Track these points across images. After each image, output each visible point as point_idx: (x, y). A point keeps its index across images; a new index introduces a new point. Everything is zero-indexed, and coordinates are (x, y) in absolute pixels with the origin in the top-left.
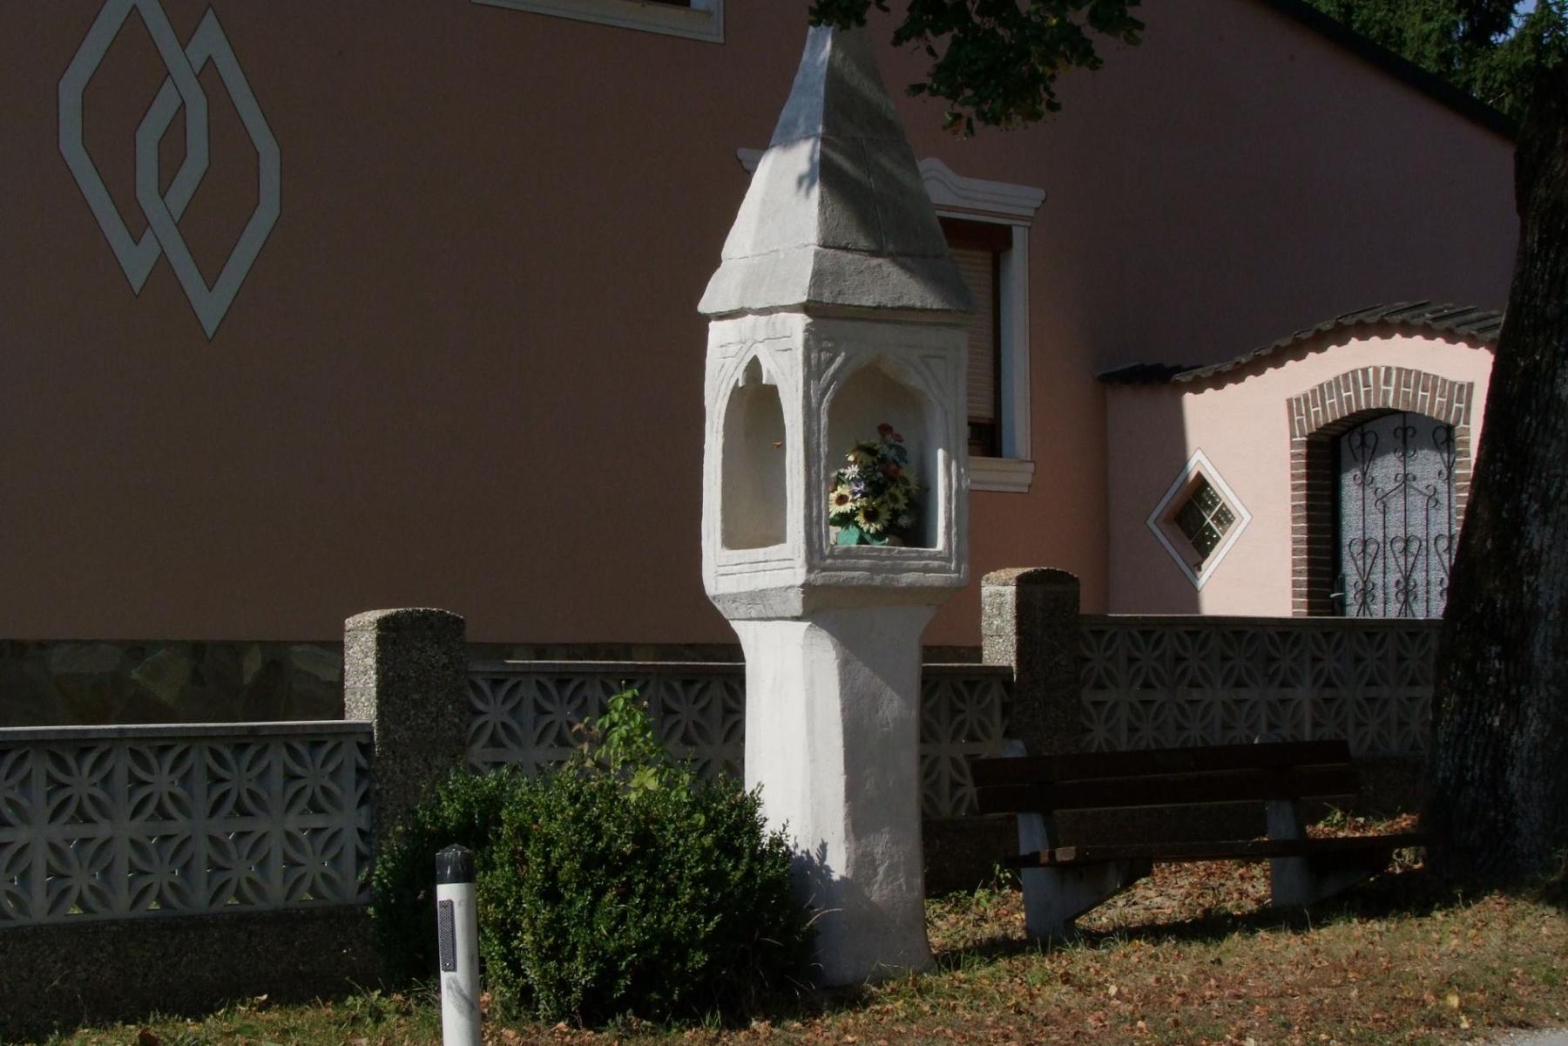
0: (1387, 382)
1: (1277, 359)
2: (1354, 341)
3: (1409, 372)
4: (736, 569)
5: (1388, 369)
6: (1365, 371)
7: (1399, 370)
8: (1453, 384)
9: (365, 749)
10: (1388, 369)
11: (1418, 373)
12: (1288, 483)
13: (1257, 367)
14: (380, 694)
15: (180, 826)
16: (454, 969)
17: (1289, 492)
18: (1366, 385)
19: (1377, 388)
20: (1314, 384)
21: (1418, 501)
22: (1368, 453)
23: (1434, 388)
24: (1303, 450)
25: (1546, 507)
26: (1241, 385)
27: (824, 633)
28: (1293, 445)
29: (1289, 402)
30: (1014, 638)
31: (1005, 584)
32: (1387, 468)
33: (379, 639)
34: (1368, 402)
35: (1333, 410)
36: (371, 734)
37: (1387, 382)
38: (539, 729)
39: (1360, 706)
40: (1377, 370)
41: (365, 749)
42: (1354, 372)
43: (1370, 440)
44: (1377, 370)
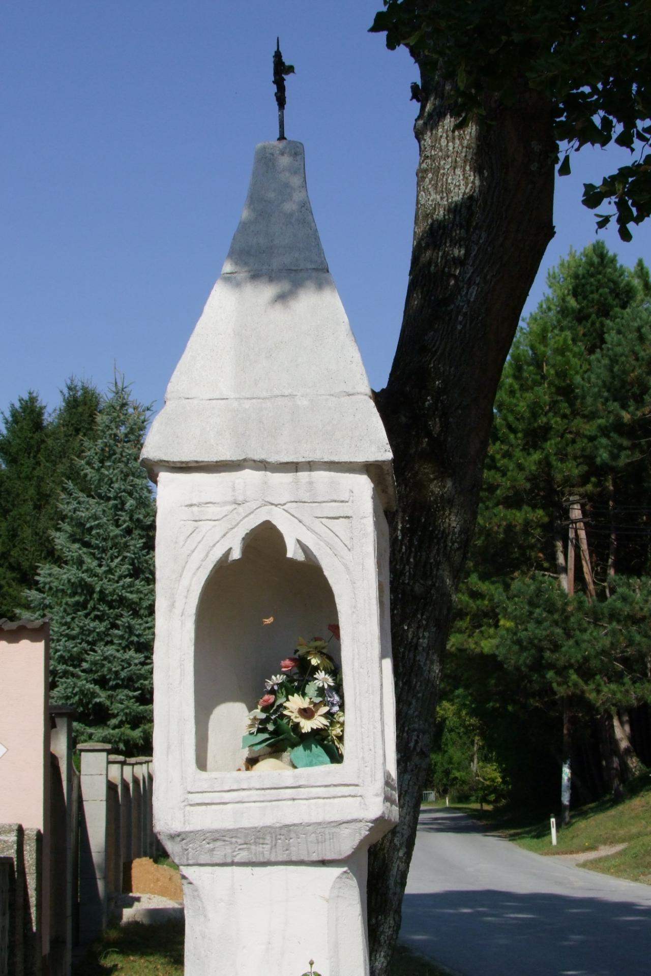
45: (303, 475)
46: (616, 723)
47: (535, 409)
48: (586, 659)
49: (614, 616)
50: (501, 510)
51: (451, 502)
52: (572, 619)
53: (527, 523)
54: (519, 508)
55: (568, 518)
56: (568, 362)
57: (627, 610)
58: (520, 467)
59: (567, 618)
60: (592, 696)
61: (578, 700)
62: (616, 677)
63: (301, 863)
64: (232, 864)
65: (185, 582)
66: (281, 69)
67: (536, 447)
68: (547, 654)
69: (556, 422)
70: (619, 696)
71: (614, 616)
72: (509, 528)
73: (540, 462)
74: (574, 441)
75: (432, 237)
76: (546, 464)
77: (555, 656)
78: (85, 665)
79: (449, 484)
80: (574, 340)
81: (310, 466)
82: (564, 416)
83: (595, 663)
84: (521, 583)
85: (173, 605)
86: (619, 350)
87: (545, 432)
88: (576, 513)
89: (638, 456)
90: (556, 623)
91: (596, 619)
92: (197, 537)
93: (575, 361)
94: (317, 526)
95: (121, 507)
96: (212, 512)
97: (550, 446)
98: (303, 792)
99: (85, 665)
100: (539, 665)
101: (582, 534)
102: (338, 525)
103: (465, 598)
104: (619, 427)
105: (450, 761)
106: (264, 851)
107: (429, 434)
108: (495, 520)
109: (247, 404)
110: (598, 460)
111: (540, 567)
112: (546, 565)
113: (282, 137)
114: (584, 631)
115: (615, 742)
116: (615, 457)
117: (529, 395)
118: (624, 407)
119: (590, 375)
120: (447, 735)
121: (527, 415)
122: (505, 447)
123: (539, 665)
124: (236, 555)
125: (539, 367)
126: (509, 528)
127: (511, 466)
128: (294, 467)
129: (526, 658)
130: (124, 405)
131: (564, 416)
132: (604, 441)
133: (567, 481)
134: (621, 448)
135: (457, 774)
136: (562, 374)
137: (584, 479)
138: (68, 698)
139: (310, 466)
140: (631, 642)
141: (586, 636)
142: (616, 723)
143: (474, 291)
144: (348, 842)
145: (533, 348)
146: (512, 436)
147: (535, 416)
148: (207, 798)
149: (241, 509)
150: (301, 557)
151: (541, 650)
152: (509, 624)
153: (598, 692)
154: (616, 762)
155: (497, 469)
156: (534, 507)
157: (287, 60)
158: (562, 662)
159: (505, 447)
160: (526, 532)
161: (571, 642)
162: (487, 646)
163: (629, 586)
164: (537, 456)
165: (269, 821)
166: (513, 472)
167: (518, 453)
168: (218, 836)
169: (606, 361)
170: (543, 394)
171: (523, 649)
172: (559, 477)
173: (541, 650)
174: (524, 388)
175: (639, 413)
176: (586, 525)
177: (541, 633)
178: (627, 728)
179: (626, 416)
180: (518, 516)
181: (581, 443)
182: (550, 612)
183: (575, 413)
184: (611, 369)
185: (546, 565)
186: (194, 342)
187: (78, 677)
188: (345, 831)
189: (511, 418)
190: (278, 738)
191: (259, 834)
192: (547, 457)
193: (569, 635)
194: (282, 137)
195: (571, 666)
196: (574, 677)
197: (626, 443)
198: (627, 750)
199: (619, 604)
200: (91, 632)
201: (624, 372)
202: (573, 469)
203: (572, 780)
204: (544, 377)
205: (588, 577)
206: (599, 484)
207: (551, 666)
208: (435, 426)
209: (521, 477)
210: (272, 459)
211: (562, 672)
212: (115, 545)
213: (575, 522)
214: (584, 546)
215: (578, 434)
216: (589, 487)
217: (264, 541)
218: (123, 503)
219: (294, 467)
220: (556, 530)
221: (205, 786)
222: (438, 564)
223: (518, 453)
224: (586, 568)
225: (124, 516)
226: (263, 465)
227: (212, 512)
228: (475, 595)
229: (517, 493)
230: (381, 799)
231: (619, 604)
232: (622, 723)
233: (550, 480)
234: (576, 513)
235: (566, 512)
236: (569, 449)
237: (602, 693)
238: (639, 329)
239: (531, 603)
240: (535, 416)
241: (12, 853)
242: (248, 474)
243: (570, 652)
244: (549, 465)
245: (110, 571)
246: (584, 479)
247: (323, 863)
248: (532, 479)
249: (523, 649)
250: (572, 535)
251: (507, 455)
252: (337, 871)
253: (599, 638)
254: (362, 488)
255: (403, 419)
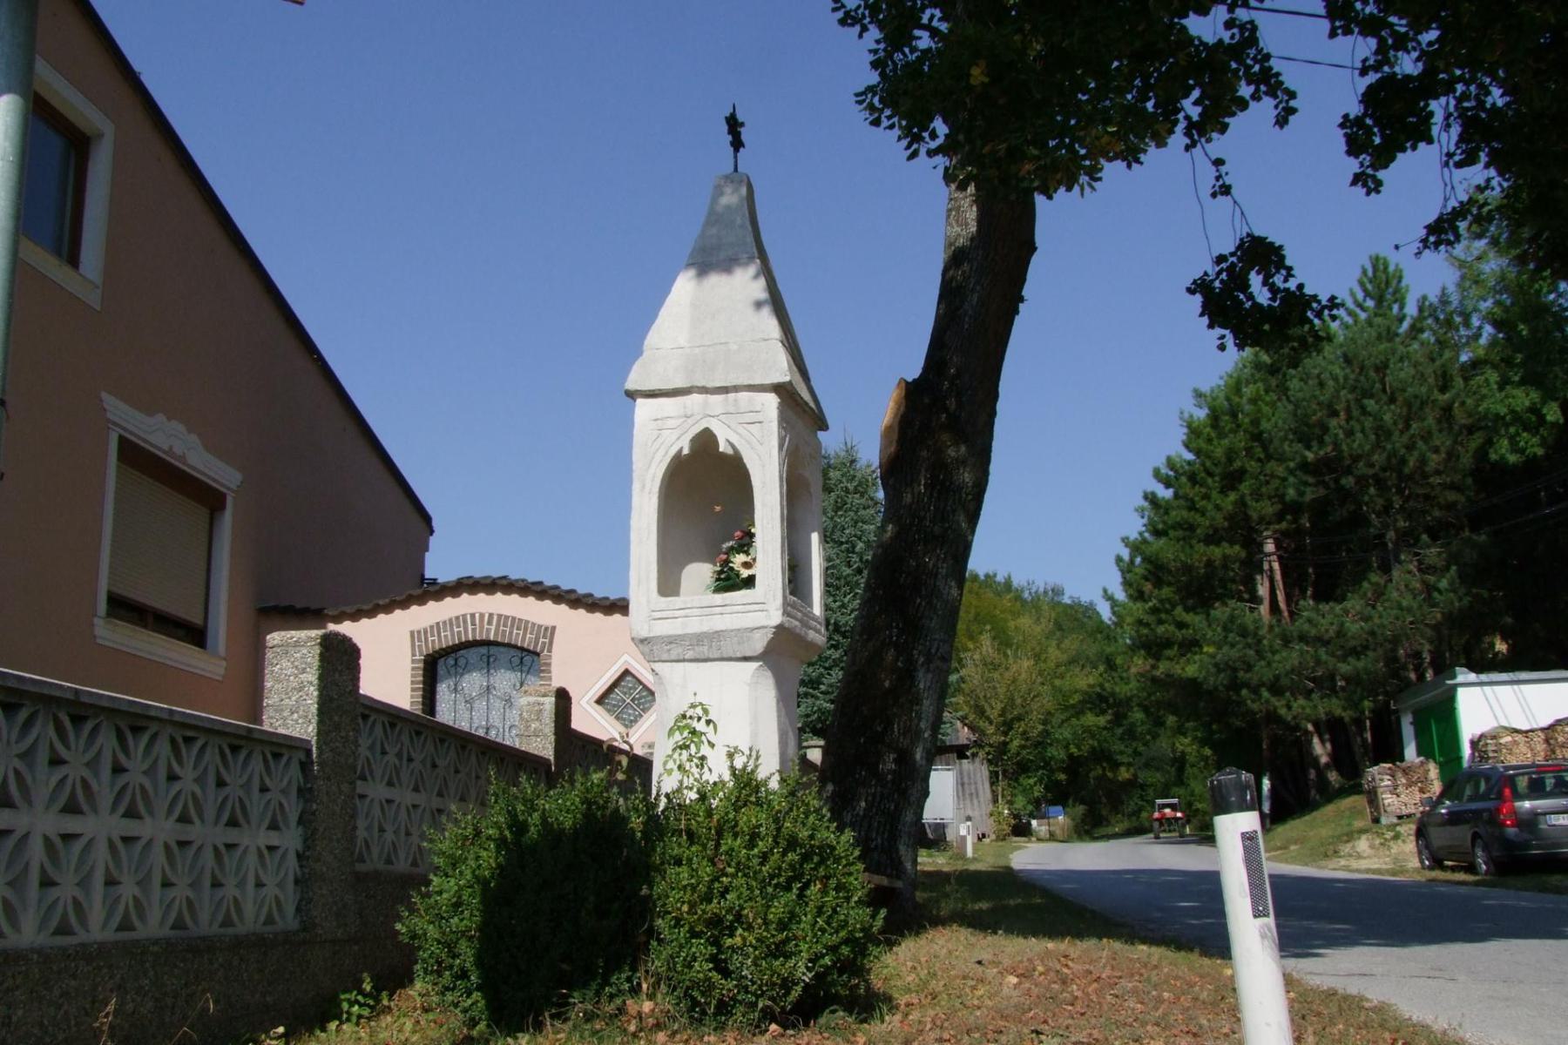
0: (490, 623)
1: (404, 604)
2: (465, 595)
3: (507, 617)
4: (678, 613)
5: (491, 615)
6: (473, 616)
7: (500, 616)
8: (540, 627)
9: (305, 766)
10: (491, 615)
11: (514, 619)
12: (408, 686)
13: (388, 609)
14: (321, 712)
15: (195, 832)
16: (1267, 915)
17: (409, 693)
18: (473, 624)
19: (482, 627)
20: (433, 621)
21: (498, 704)
22: (459, 670)
23: (526, 629)
24: (421, 665)
25: (929, 661)
26: (373, 620)
27: (769, 674)
28: (413, 661)
29: (412, 633)
30: (552, 738)
31: (545, 695)
32: (473, 681)
33: (321, 655)
34: (496, 634)
35: (447, 639)
36: (309, 752)
37: (490, 623)
38: (171, 796)
39: (261, 855)
40: (482, 616)
41: (305, 766)
42: (464, 616)
43: (462, 662)
44: (482, 616)
45: (732, 396)
46: (1316, 740)
47: (1231, 455)
48: (1277, 678)
49: (1303, 638)
50: (1201, 547)
51: (964, 463)
52: (1265, 642)
53: (1225, 557)
54: (1218, 544)
55: (1261, 551)
56: (1259, 411)
57: (1313, 632)
58: (1218, 508)
59: (1260, 641)
60: (1283, 711)
61: (1272, 717)
62: (1308, 694)
63: (730, 659)
64: (684, 660)
65: (652, 471)
66: (734, 124)
67: (1233, 488)
68: (1241, 674)
69: (1252, 466)
70: (1308, 711)
71: (1303, 638)
72: (1209, 563)
73: (1235, 503)
74: (1268, 483)
75: (956, 258)
76: (1241, 503)
77: (1248, 675)
78: (823, 688)
79: (963, 449)
80: (1267, 392)
81: (736, 389)
82: (1259, 460)
83: (1285, 681)
84: (1220, 612)
85: (644, 487)
86: (1300, 395)
87: (1240, 475)
88: (1270, 547)
89: (1322, 492)
90: (1249, 646)
91: (1287, 641)
92: (660, 440)
93: (1266, 409)
94: (741, 429)
95: (852, 550)
96: (671, 423)
97: (1245, 487)
98: (728, 609)
99: (823, 688)
100: (1235, 685)
101: (1276, 566)
102: (754, 428)
103: (1172, 628)
104: (1304, 466)
105: (1192, 794)
106: (704, 651)
107: (946, 410)
108: (1196, 557)
109: (697, 351)
110: (1288, 498)
111: (1241, 599)
112: (1246, 596)
113: (736, 169)
114: (1274, 653)
115: (1316, 760)
116: (1302, 494)
117: (1226, 442)
118: (1309, 448)
119: (1277, 420)
120: (1189, 770)
121: (1223, 460)
122: (1203, 490)
123: (1235, 685)
124: (686, 451)
125: (1234, 415)
126: (1209, 563)
127: (1210, 507)
128: (724, 390)
129: (1223, 678)
130: (853, 462)
131: (1259, 460)
132: (1291, 479)
133: (1261, 519)
134: (1306, 484)
135: (1199, 806)
136: (1255, 422)
137: (1280, 517)
138: (807, 716)
139: (736, 389)
140: (1318, 662)
141: (1277, 657)
142: (1316, 740)
143: (975, 297)
144: (759, 644)
145: (1228, 399)
146: (1210, 480)
147: (1230, 460)
148: (664, 614)
149: (690, 421)
150: (730, 451)
151: (1235, 670)
152: (1211, 650)
153: (1289, 708)
154: (1312, 774)
155: (1197, 510)
156: (1232, 543)
157: (740, 118)
158: (1255, 681)
159: (1203, 490)
160: (1225, 567)
161: (1263, 663)
162: (1191, 671)
163: (1318, 610)
164: (1232, 496)
165: (705, 629)
166: (1211, 512)
167: (1215, 494)
168: (672, 640)
169: (1291, 407)
170: (1240, 441)
171: (1219, 671)
172: (1255, 516)
173: (1235, 670)
174: (1222, 435)
175: (1322, 453)
176: (1280, 559)
177: (1234, 653)
178: (1328, 746)
179: (1310, 456)
180: (1216, 552)
181: (1275, 483)
182: (1243, 636)
183: (1269, 457)
184: (1295, 415)
185: (1246, 596)
186: (663, 312)
187: (817, 698)
188: (757, 635)
189: (1208, 464)
190: (729, 581)
191: (699, 639)
192: (1242, 497)
193: (1260, 654)
194: (736, 169)
195: (1263, 685)
196: (1265, 694)
197: (1311, 480)
198: (1327, 765)
199: (1306, 627)
200: (827, 659)
201: (1306, 415)
202: (1269, 509)
203: (1273, 789)
204: (1239, 426)
205: (1282, 605)
206: (1295, 521)
207: (1246, 685)
208: (952, 404)
209: (1219, 517)
210: (711, 385)
211: (1255, 690)
212: (847, 584)
213: (1270, 554)
214: (1278, 576)
215: (1273, 476)
216: (1284, 525)
217: (705, 441)
218: (854, 547)
219: (724, 390)
220: (1253, 565)
221: (663, 606)
222: (954, 511)
223: (1215, 494)
224: (1281, 597)
225: (855, 558)
226: (704, 390)
227: (671, 423)
228: (1181, 625)
229: (1216, 530)
230: (780, 612)
231: (1306, 627)
232: (1323, 742)
233: (1247, 518)
234: (1270, 547)
235: (1261, 545)
236: (1264, 490)
237: (1300, 709)
238: (1318, 376)
239: (1225, 629)
240: (1230, 460)
241: (439, 564)
242: (695, 397)
243: (1262, 672)
244: (1244, 504)
245: (843, 606)
246: (1280, 517)
247: (746, 659)
248: (1230, 518)
249: (1219, 671)
250: (1266, 566)
251: (1206, 497)
252: (755, 665)
253: (1290, 658)
254: (771, 401)
255: (926, 401)
